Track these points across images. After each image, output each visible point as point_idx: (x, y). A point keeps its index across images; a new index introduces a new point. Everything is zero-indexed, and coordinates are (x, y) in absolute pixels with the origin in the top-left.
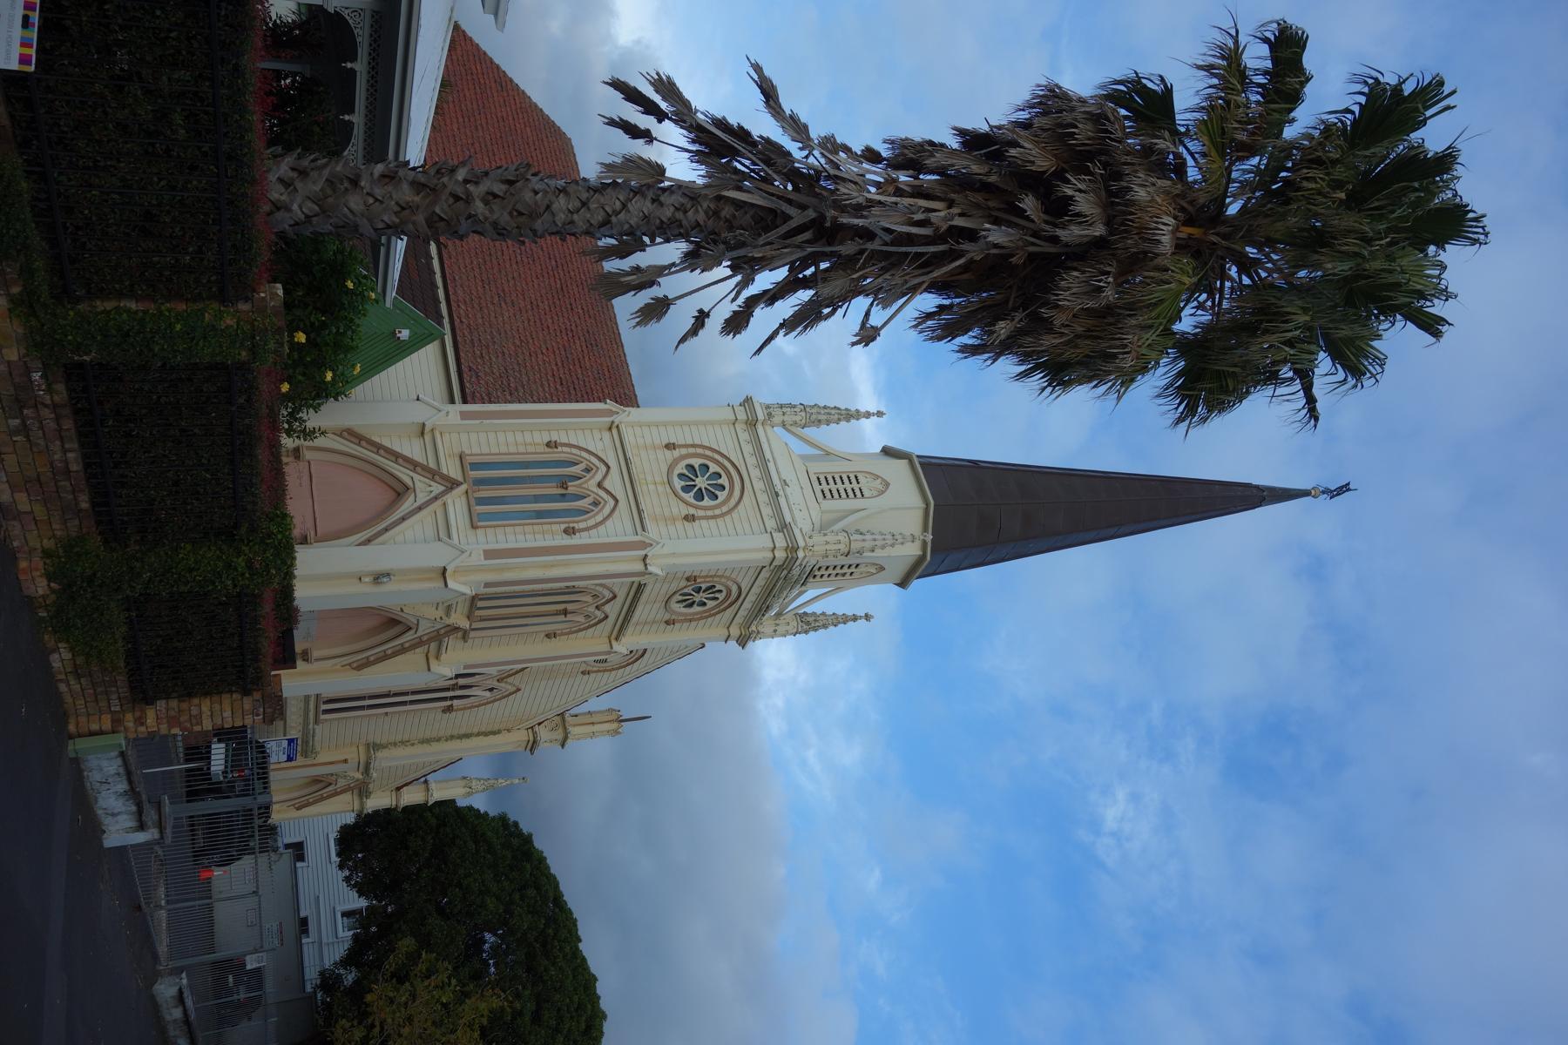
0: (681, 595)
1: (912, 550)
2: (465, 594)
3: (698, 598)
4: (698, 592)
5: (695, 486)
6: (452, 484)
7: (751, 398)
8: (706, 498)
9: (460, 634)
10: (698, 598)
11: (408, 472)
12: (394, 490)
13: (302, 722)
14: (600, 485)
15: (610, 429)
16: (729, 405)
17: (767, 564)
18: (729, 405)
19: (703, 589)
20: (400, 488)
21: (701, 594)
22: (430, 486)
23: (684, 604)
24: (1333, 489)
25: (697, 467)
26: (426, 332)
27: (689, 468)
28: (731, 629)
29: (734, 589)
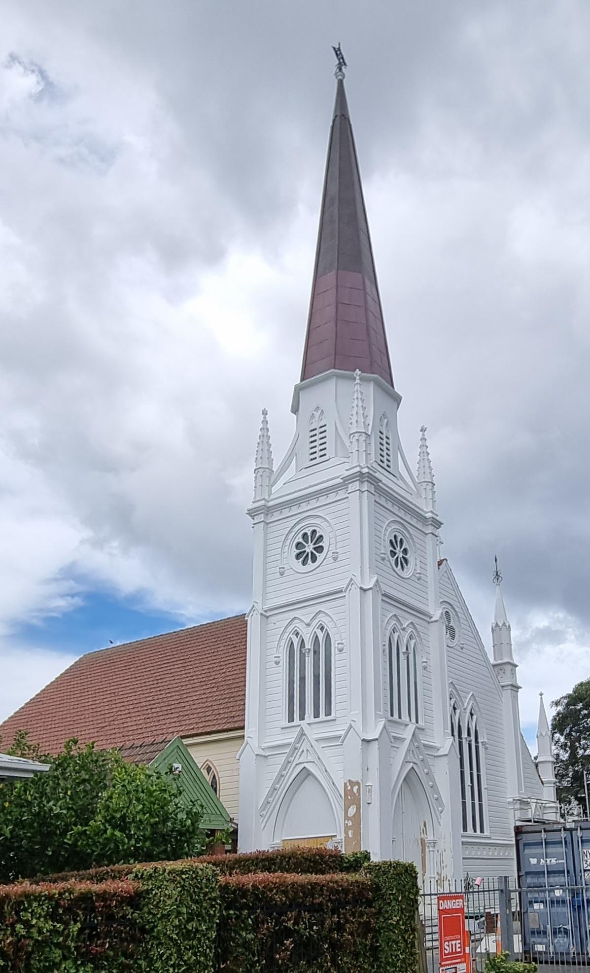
0: (397, 567)
2: (384, 727)
4: (395, 554)
5: (312, 553)
6: (302, 734)
8: (320, 544)
12: (306, 778)
15: (267, 617)
16: (253, 527)
17: (373, 498)
18: (253, 527)
19: (392, 549)
21: (397, 551)
22: (303, 751)
23: (404, 565)
24: (337, 62)
25: (298, 551)
26: (175, 750)
27: (305, 562)
28: (427, 532)
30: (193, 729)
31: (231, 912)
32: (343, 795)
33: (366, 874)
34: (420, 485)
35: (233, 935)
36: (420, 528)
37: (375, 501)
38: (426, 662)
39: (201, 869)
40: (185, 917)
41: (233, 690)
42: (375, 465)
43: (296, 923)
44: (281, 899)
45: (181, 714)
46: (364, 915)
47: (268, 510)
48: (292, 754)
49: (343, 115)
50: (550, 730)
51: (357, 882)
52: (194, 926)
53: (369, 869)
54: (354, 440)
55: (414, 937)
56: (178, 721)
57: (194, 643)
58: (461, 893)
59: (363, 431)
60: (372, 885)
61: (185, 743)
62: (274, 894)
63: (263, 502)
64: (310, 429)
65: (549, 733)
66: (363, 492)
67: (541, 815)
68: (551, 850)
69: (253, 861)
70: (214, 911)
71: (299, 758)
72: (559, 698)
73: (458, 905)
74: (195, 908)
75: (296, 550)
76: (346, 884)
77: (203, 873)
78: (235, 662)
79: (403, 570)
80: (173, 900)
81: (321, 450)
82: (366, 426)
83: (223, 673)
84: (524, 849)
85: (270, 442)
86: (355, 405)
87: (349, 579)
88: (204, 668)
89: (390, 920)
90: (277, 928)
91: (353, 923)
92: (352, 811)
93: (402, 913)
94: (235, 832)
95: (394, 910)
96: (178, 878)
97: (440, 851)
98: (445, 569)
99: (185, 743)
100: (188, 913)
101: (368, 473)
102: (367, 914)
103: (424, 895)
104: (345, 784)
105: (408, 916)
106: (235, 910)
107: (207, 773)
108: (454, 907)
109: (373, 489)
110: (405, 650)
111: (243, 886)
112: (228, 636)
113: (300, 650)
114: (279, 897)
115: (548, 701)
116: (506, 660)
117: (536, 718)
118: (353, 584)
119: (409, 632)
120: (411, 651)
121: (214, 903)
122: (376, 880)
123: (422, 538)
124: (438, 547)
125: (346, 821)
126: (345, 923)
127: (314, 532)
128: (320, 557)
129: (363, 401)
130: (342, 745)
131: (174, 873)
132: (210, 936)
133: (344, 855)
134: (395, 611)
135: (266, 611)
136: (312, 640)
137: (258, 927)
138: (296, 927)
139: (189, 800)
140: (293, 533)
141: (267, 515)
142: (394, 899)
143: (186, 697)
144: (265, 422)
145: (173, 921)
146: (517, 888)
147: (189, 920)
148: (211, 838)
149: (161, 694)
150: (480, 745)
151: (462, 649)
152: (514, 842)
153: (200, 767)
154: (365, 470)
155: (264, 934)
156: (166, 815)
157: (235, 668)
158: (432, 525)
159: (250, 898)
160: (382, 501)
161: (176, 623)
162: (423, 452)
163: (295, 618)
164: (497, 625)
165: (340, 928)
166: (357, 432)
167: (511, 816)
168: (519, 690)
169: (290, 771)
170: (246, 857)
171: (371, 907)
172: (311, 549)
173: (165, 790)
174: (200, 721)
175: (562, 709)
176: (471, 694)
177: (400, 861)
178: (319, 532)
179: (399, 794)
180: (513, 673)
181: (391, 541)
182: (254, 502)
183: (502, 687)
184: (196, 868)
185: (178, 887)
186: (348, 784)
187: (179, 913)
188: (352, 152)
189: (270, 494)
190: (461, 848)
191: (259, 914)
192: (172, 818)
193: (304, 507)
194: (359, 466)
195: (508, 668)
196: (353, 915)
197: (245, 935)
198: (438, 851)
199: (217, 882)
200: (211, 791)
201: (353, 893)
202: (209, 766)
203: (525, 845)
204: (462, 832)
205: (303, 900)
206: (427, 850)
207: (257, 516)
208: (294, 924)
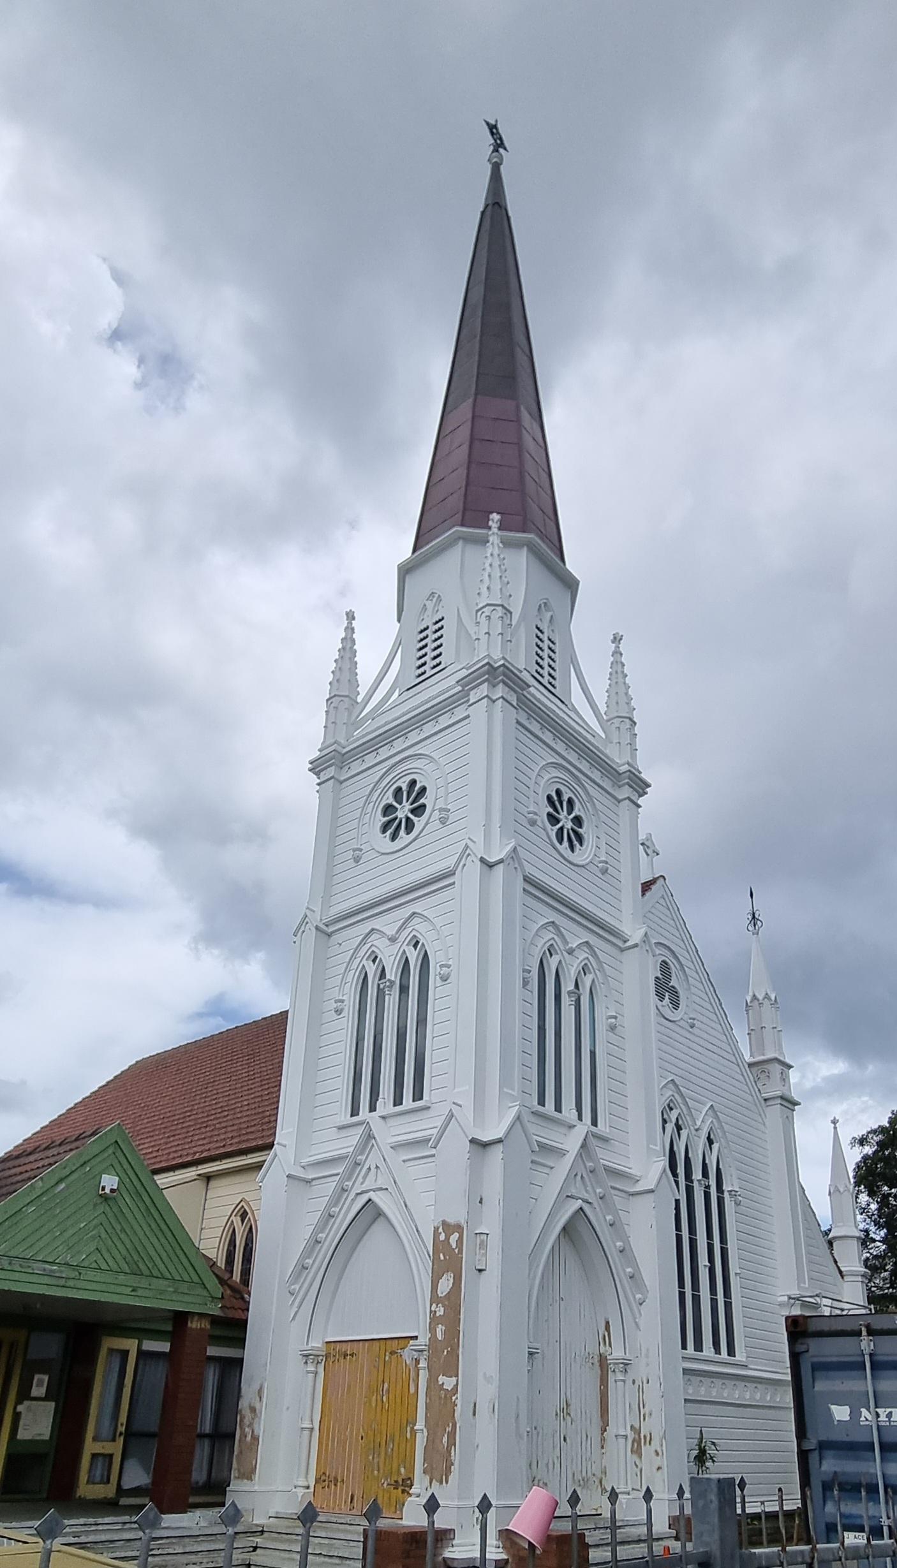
0: (561, 842)
1: (521, 559)
2: (518, 1118)
5: (408, 819)
6: (370, 1136)
7: (311, 763)
8: (422, 801)
9: (593, 1142)
11: (350, 1199)
13: (699, 1378)
14: (393, 940)
19: (551, 810)
20: (369, 1213)
22: (369, 1169)
23: (575, 842)
26: (110, 1151)
28: (620, 798)
34: (609, 723)
37: (518, 722)
38: (615, 1018)
48: (349, 1175)
49: (497, 203)
54: (483, 620)
59: (499, 602)
64: (419, 630)
71: (362, 1183)
72: (865, 1132)
79: (573, 851)
92: (445, 1285)
98: (662, 892)
104: (436, 1229)
110: (571, 987)
116: (770, 1055)
118: (469, 855)
119: (581, 958)
123: (613, 807)
125: (434, 1305)
134: (553, 917)
135: (327, 926)
136: (397, 968)
141: (341, 768)
150: (726, 1195)
162: (617, 662)
166: (488, 605)
169: (346, 1206)
178: (421, 782)
179: (548, 1257)
180: (785, 1079)
181: (549, 798)
186: (441, 1230)
188: (509, 248)
198: (634, 1382)
202: (245, 1211)
203: (817, 1367)
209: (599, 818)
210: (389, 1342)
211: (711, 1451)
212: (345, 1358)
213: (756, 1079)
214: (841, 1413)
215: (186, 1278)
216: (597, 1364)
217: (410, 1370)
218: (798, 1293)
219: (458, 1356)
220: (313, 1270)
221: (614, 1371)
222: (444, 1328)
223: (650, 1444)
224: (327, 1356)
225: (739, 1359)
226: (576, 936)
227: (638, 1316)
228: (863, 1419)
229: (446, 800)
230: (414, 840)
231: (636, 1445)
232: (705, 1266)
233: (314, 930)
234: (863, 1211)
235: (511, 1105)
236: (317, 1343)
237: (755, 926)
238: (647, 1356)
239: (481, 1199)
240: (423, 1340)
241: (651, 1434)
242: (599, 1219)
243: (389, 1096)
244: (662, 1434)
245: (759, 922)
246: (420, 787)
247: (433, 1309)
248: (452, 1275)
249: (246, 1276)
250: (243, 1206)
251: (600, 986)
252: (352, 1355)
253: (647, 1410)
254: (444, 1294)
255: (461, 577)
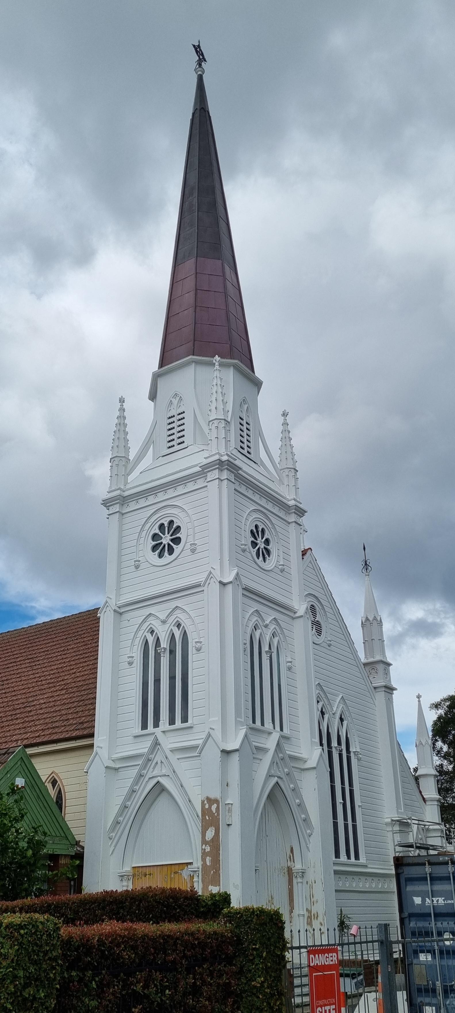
0: (258, 559)
1: (230, 375)
2: (246, 736)
3: (261, 545)
4: (256, 544)
5: (169, 545)
6: (156, 744)
7: (103, 501)
8: (178, 535)
9: (282, 741)
10: (261, 545)
14: (164, 622)
15: (121, 614)
16: (108, 518)
17: (233, 486)
18: (108, 518)
19: (253, 539)
21: (258, 542)
22: (157, 763)
23: (266, 556)
24: (198, 58)
26: (19, 763)
28: (290, 521)
29: (255, 515)
30: (39, 736)
31: (74, 974)
32: (200, 815)
33: (225, 923)
34: (282, 471)
35: (75, 1002)
36: (282, 517)
37: (235, 490)
38: (291, 662)
39: (41, 922)
40: (22, 982)
41: (82, 693)
42: (235, 452)
43: (146, 986)
44: (129, 956)
45: (27, 719)
46: (223, 975)
47: (123, 500)
48: (144, 766)
49: (203, 108)
50: (431, 737)
51: (215, 933)
52: (32, 993)
53: (229, 916)
54: (213, 427)
55: (281, 1004)
56: (23, 728)
57: (43, 640)
58: (334, 945)
60: (233, 937)
61: (28, 753)
62: (122, 950)
63: (118, 492)
65: (430, 742)
66: (222, 480)
67: (424, 839)
68: (438, 887)
69: (100, 904)
70: (55, 974)
72: (439, 700)
73: (332, 961)
74: (33, 970)
75: (152, 542)
76: (202, 937)
77: (43, 927)
78: (85, 662)
79: (265, 561)
80: (9, 961)
81: (179, 438)
82: (226, 412)
83: (73, 673)
84: (410, 924)
85: (127, 429)
86: (214, 391)
87: (208, 572)
88: (53, 667)
89: (253, 981)
90: (124, 993)
91: (211, 985)
92: (210, 834)
93: (267, 972)
94: (80, 856)
95: (258, 969)
96: (16, 934)
97: (310, 883)
99: (28, 753)
100: (25, 977)
101: (228, 460)
102: (227, 974)
103: (292, 948)
104: (203, 802)
105: (274, 977)
106: (77, 971)
107: (52, 787)
108: (326, 964)
109: (233, 477)
110: (267, 649)
111: (88, 941)
112: (80, 633)
113: (156, 650)
114: (127, 954)
115: (426, 703)
116: (378, 658)
117: (414, 721)
118: (212, 577)
119: (272, 629)
120: (274, 650)
121: (54, 964)
122: (237, 931)
124: (301, 535)
126: (202, 985)
127: (171, 522)
128: (177, 549)
129: (222, 387)
130: (200, 756)
131: (11, 928)
132: (48, 1004)
133: (201, 898)
135: (119, 608)
137: (103, 992)
138: (146, 991)
139: (30, 827)
140: (149, 524)
141: (123, 505)
142: (258, 955)
143: (33, 701)
144: (122, 410)
145: (8, 987)
146: (400, 939)
147: (26, 986)
148: (54, 872)
149: (6, 697)
150: (352, 755)
151: (329, 646)
152: (393, 872)
153: (44, 781)
154: (225, 458)
155: (110, 1001)
156: (5, 844)
157: (85, 668)
158: (295, 513)
159: (96, 955)
160: (243, 489)
161: (25, 617)
163: (150, 614)
164: (367, 619)
165: (195, 991)
167: (391, 847)
168: (394, 692)
170: (92, 898)
171: (231, 964)
172: (168, 541)
173: (6, 814)
174: (47, 727)
175: (443, 713)
176: (340, 697)
177: (264, 907)
181: (252, 532)
182: (109, 492)
183: (375, 688)
184: (36, 922)
185: (15, 945)
186: (206, 802)
187: (15, 977)
188: (211, 143)
189: (126, 483)
190: (333, 878)
191: (104, 976)
192: (12, 848)
193: (161, 496)
194: (218, 453)
195: (381, 667)
196: (211, 974)
197: (88, 1002)
198: (307, 883)
199: (59, 938)
200: (55, 808)
201: (212, 947)
204: (334, 859)
205: (154, 957)
206: (295, 881)
207: (112, 507)
208: (144, 987)
209: (279, 537)
210: (173, 867)
211: (347, 922)
212: (145, 876)
213: (369, 674)
214: (418, 900)
215: (58, 834)
216: (286, 873)
217: (187, 882)
218: (397, 816)
219: (220, 874)
220: (123, 825)
221: (296, 877)
222: (210, 858)
223: (317, 919)
224: (134, 876)
225: (362, 862)
226: (269, 616)
227: (308, 842)
228: (427, 903)
229: (194, 537)
230: (175, 559)
231: (309, 919)
232: (340, 803)
233: (112, 612)
234: (439, 752)
235: (241, 728)
236: (127, 868)
237: (367, 570)
238: (314, 867)
239: (227, 784)
240: (198, 864)
241: (317, 913)
242: (287, 787)
243: (166, 720)
244: (323, 912)
245: (369, 567)
246: (176, 527)
247: (203, 847)
248: (214, 828)
249: (216, 865)
250: (53, 776)
251: (282, 643)
252: (150, 874)
253: (315, 899)
254: (210, 839)
255: (195, 388)
